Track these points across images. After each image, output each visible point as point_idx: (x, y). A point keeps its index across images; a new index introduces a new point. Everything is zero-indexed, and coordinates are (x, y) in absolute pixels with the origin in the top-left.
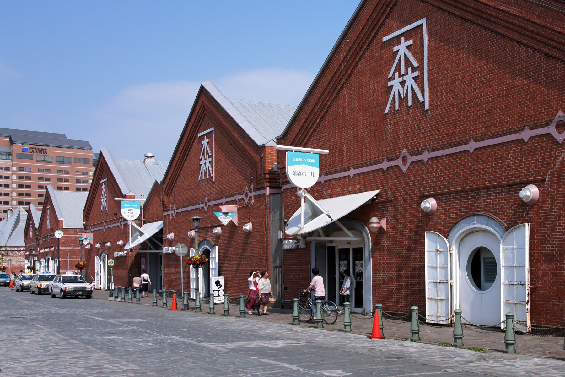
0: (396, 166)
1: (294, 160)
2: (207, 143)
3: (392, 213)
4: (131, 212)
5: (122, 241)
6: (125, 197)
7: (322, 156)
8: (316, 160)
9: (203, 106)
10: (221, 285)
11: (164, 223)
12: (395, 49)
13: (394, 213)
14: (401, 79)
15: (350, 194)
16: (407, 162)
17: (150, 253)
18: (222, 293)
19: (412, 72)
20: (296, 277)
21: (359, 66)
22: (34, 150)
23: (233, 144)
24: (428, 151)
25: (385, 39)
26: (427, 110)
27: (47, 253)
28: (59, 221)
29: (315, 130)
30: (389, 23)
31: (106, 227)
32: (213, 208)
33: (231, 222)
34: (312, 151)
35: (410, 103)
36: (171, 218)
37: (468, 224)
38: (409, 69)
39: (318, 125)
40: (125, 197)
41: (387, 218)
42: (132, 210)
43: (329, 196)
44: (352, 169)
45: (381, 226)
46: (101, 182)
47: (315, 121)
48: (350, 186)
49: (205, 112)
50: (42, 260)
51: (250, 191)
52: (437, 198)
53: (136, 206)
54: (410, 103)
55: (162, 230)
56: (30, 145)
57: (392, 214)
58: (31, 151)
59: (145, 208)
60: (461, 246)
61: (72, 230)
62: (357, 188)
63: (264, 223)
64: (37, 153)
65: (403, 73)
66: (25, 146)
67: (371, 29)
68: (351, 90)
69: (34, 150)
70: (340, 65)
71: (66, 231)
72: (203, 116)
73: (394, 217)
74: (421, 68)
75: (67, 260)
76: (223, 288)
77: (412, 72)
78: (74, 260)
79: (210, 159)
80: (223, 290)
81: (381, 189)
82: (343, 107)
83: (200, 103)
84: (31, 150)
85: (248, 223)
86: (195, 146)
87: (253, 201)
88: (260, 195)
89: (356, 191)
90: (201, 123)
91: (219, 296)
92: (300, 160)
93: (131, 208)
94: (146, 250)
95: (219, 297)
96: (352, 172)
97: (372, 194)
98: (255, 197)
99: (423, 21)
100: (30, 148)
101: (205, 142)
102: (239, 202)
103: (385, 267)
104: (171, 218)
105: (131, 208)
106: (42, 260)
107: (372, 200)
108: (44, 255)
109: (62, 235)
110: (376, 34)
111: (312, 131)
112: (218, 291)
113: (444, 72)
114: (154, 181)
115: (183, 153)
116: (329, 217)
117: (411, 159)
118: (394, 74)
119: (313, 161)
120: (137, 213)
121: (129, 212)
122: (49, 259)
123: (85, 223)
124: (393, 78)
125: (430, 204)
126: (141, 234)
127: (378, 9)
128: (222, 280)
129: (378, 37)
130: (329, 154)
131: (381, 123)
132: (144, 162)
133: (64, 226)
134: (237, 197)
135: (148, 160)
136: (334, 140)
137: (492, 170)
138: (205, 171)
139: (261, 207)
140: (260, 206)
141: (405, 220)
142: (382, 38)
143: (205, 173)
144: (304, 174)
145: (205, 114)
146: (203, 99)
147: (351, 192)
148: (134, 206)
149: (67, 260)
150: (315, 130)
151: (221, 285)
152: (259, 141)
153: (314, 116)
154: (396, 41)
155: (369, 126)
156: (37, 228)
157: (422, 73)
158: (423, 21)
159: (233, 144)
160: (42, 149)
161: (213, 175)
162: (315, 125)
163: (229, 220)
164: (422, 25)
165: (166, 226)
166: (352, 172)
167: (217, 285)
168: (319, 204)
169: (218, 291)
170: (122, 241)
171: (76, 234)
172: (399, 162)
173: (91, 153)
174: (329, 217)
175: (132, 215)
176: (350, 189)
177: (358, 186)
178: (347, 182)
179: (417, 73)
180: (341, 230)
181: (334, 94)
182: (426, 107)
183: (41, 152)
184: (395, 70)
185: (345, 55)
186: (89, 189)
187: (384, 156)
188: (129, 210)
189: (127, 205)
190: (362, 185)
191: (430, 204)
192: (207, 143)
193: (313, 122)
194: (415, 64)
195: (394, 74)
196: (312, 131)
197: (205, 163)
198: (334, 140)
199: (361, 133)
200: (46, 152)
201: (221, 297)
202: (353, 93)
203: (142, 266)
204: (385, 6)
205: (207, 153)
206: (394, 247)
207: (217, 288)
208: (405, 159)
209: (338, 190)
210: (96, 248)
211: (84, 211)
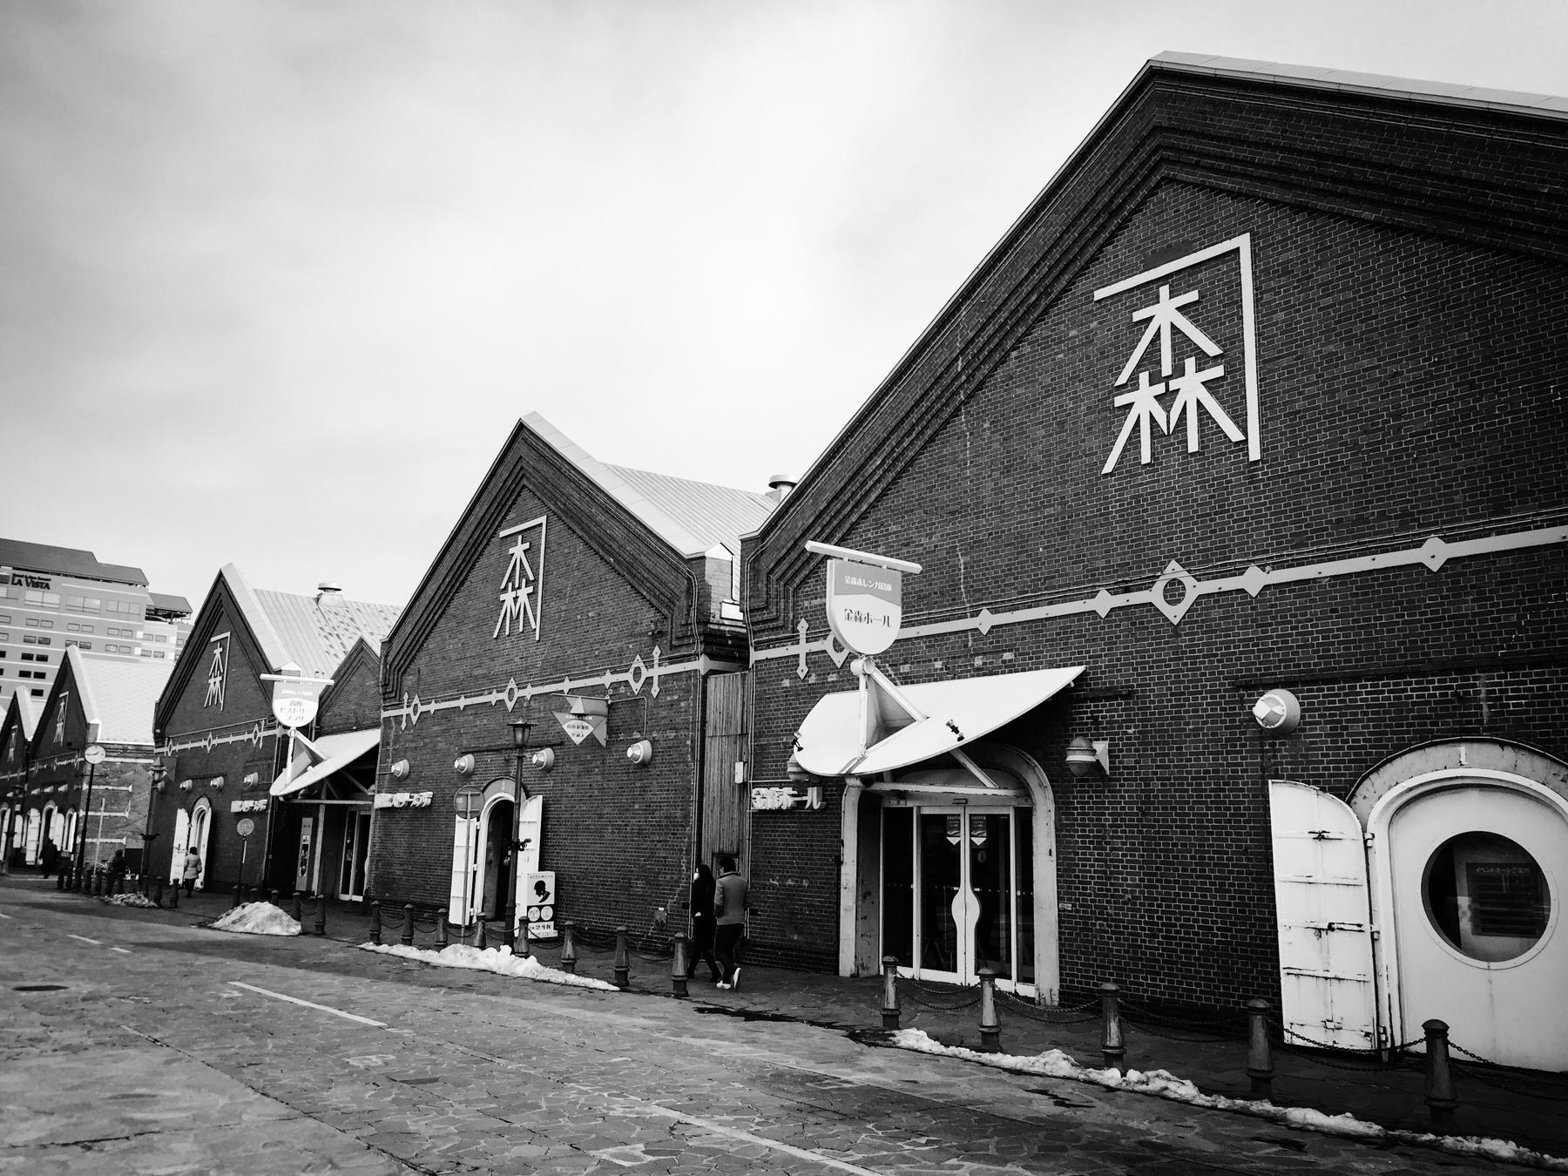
0: (1089, 613)
1: (847, 582)
2: (525, 551)
3: (1129, 728)
4: (298, 708)
5: (256, 774)
6: (279, 672)
7: (906, 576)
8: (892, 587)
9: (518, 468)
10: (549, 894)
11: (385, 737)
12: (1138, 316)
13: (1136, 727)
14: (1160, 388)
15: (978, 676)
16: (1183, 595)
17: (327, 805)
18: (548, 913)
19: (1199, 369)
20: (790, 882)
21: (1012, 363)
22: (23, 580)
23: (601, 553)
24: (1263, 568)
25: (1099, 294)
26: (1256, 462)
27: (48, 797)
28: (87, 725)
29: (863, 517)
30: (1118, 251)
31: (216, 742)
32: (532, 703)
33: (591, 739)
34: (885, 563)
35: (1193, 446)
36: (404, 725)
37: (947, 783)
38: (1190, 363)
39: (872, 506)
40: (279, 672)
41: (1111, 740)
42: (299, 704)
43: (904, 678)
44: (1253, 571)
45: (1098, 761)
46: (213, 639)
47: (864, 497)
48: (978, 655)
49: (525, 482)
50: (34, 813)
51: (649, 665)
52: (1302, 691)
53: (311, 694)
54: (1193, 446)
55: (376, 748)
56: (14, 568)
57: (1130, 731)
58: (16, 581)
59: (326, 700)
60: (1394, 826)
61: (116, 746)
62: (1004, 662)
63: (689, 742)
64: (28, 585)
65: (1167, 369)
66: (5, 570)
67: (1055, 272)
68: (984, 421)
69: (23, 580)
70: (956, 359)
71: (108, 749)
72: (517, 490)
73: (1138, 738)
74: (1232, 358)
75: (98, 814)
76: (551, 900)
77: (1199, 369)
78: (113, 814)
79: (530, 589)
80: (551, 906)
81: (1087, 663)
82: (954, 462)
83: (511, 459)
84: (17, 579)
85: (637, 741)
86: (490, 556)
87: (655, 690)
88: (1314, 580)
89: (1000, 667)
90: (510, 507)
91: (540, 920)
92: (292, 692)
93: (296, 700)
94: (319, 799)
95: (541, 924)
96: (986, 621)
97: (1063, 677)
98: (664, 679)
99: (1243, 242)
100: (15, 575)
101: (218, 651)
102: (614, 689)
103: (1105, 872)
104: (404, 725)
105: (296, 700)
106: (34, 813)
107: (1065, 693)
108: (39, 803)
109: (894, 632)
110: (1071, 283)
111: (854, 518)
112: (540, 908)
113: (1317, 365)
114: (350, 645)
115: (452, 574)
116: (955, 730)
117: (628, 676)
118: (1134, 378)
119: (889, 588)
120: (309, 713)
121: (293, 707)
122: (50, 812)
123: (158, 731)
124: (505, 590)
125: (1275, 706)
126: (316, 760)
127: (1084, 222)
128: (549, 879)
129: (1081, 286)
130: (922, 572)
131: (1089, 497)
132: (317, 600)
133: (99, 738)
134: (608, 679)
135: (326, 597)
136: (924, 541)
137: (1521, 617)
138: (515, 616)
139: (683, 704)
140: (679, 700)
141: (1180, 748)
142: (1093, 291)
143: (213, 697)
144: (868, 619)
145: (524, 487)
146: (521, 448)
147: (979, 669)
148: (306, 693)
149: (98, 814)
150: (863, 517)
151: (549, 894)
152: (687, 547)
153: (863, 484)
154: (1148, 294)
155: (1045, 507)
156: (30, 739)
157: (535, 588)
158: (1243, 242)
159: (601, 553)
160: (39, 578)
161: (535, 625)
162: (865, 507)
163: (586, 733)
164: (1236, 251)
165: (388, 744)
166: (986, 621)
167: (539, 894)
168: (908, 697)
169: (540, 908)
170: (256, 774)
171: (124, 757)
172: (628, 676)
173: (146, 592)
174: (955, 730)
175: (298, 714)
176: (978, 662)
177: (1008, 656)
178: (966, 646)
179: (1218, 371)
180: (962, 767)
181: (929, 432)
182: (1255, 453)
183: (36, 585)
184: (1140, 367)
185: (969, 338)
186: (47, 694)
187: (1098, 580)
188: (291, 704)
189: (288, 692)
190: (1020, 654)
191: (1275, 706)
192: (525, 551)
193: (858, 497)
194: (1212, 349)
195: (1134, 378)
196: (854, 518)
197: (516, 599)
198: (924, 541)
199: (1018, 523)
200: (47, 586)
201: (546, 924)
202: (989, 429)
203: (304, 837)
204: (1104, 216)
205: (523, 574)
206: (1139, 820)
207: (537, 900)
208: (637, 673)
209: (938, 665)
210: (184, 789)
211: (158, 705)
